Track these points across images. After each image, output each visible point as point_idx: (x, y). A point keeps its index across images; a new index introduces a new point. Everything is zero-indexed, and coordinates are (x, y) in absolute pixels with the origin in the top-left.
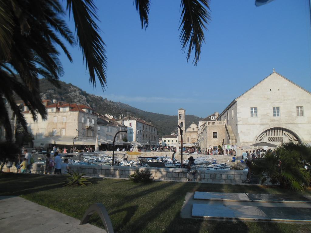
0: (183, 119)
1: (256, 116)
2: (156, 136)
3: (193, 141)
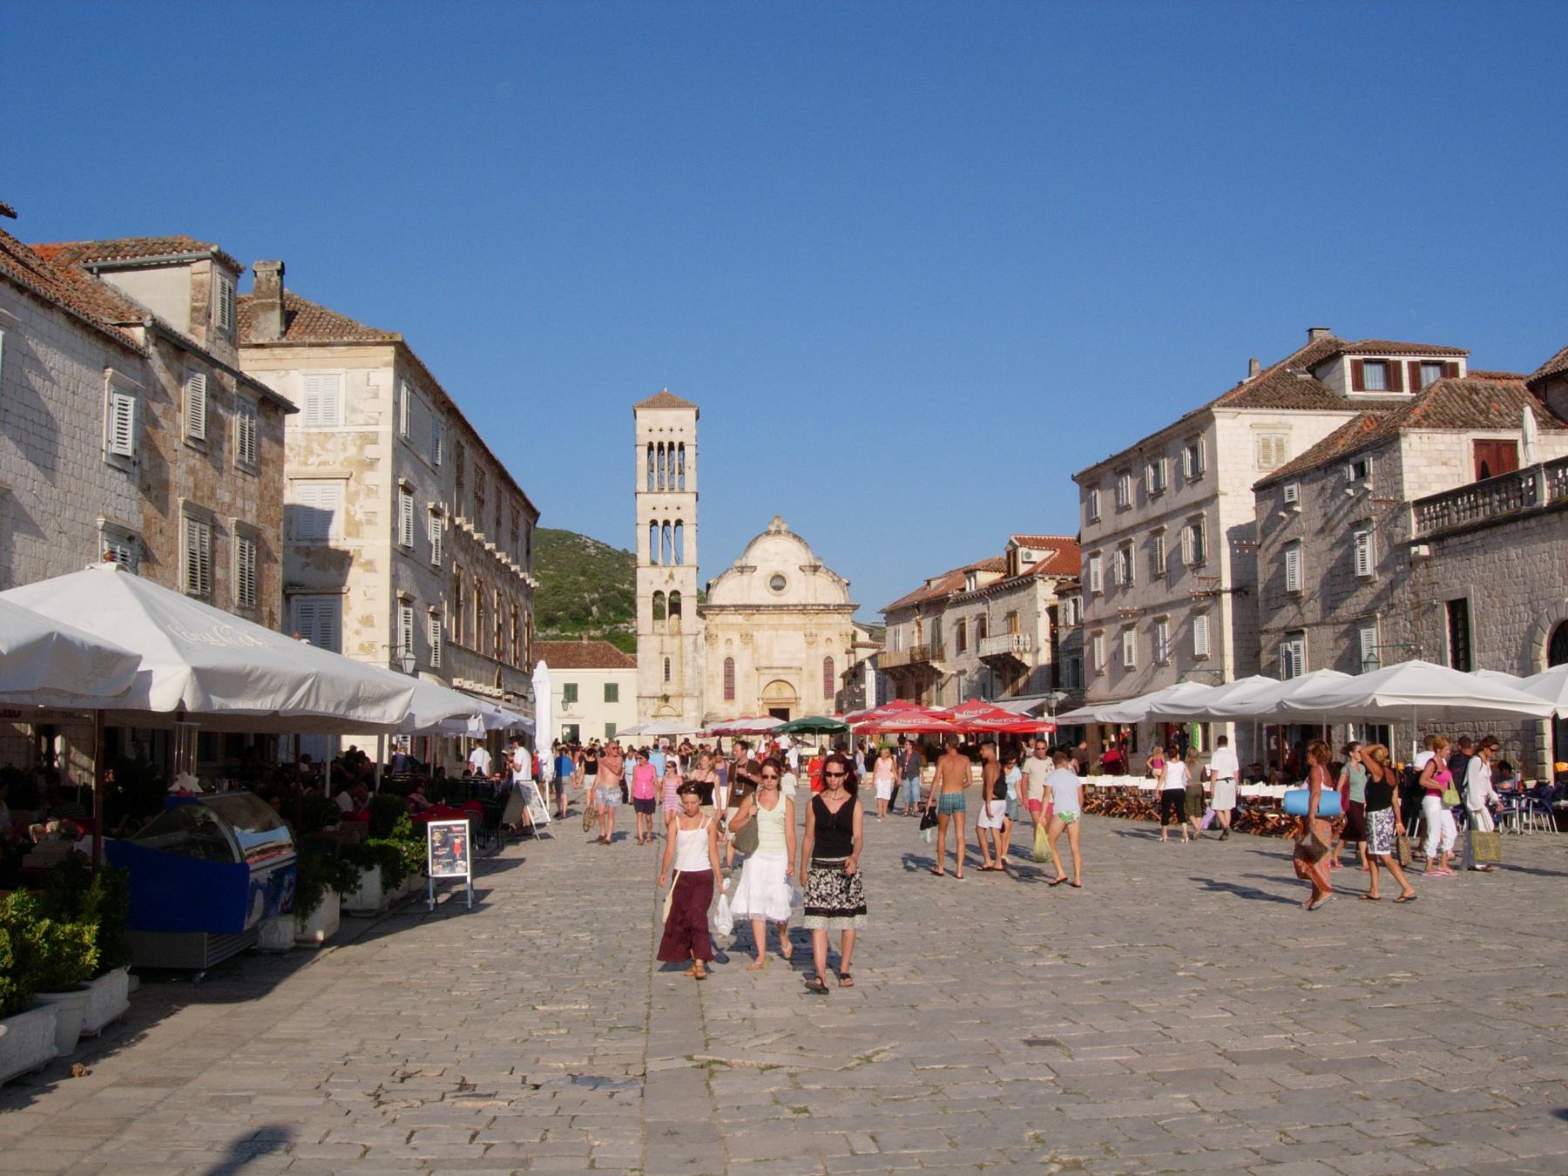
0: (682, 491)
2: (1422, 566)
3: (773, 693)
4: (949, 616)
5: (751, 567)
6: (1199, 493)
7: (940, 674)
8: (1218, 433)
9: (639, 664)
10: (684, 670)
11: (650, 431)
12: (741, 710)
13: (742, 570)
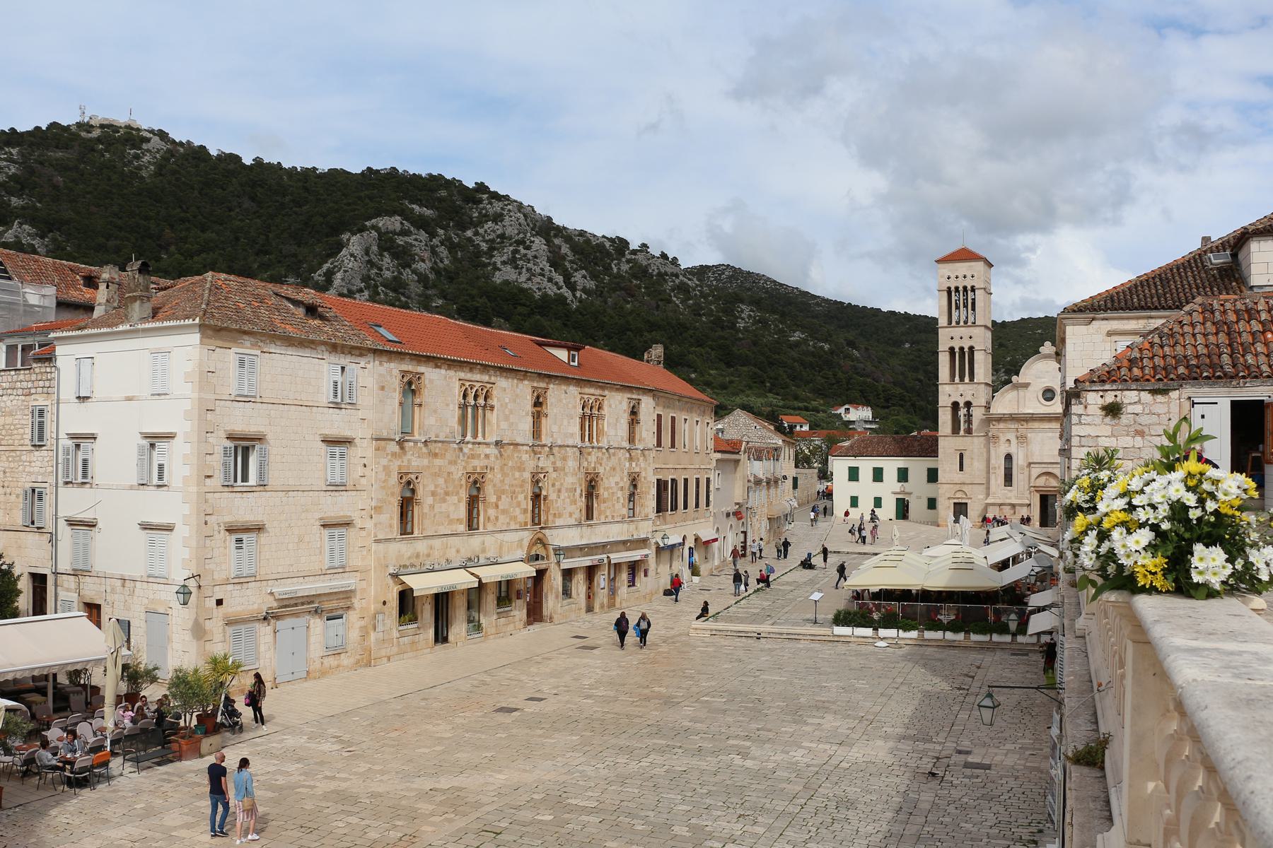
1: (95, 438)
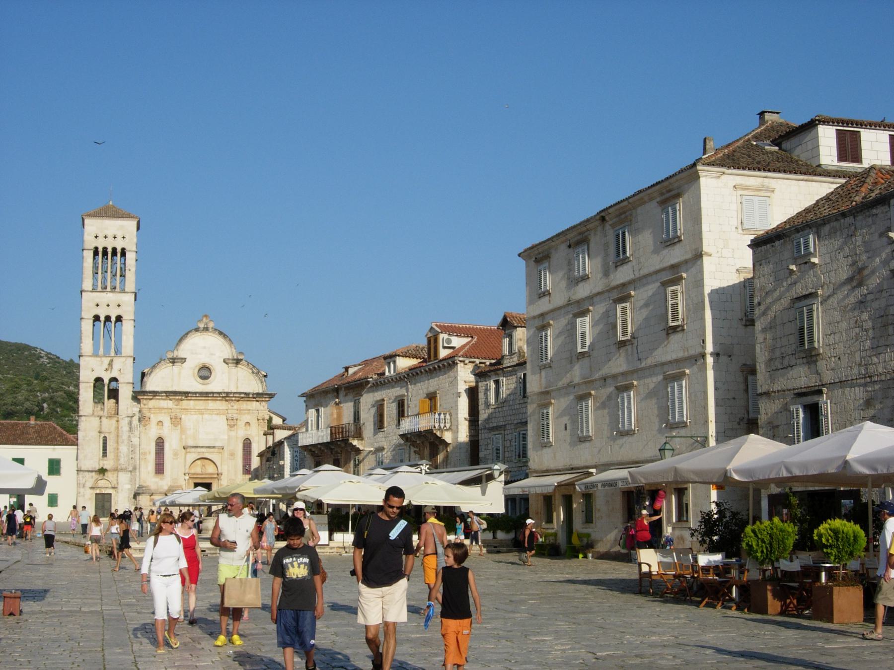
0: (123, 291)
3: (198, 469)
4: (368, 400)
5: (182, 359)
6: (675, 255)
7: (358, 451)
8: (702, 191)
9: (80, 441)
10: (120, 448)
11: (96, 237)
12: (169, 484)
13: (173, 361)
